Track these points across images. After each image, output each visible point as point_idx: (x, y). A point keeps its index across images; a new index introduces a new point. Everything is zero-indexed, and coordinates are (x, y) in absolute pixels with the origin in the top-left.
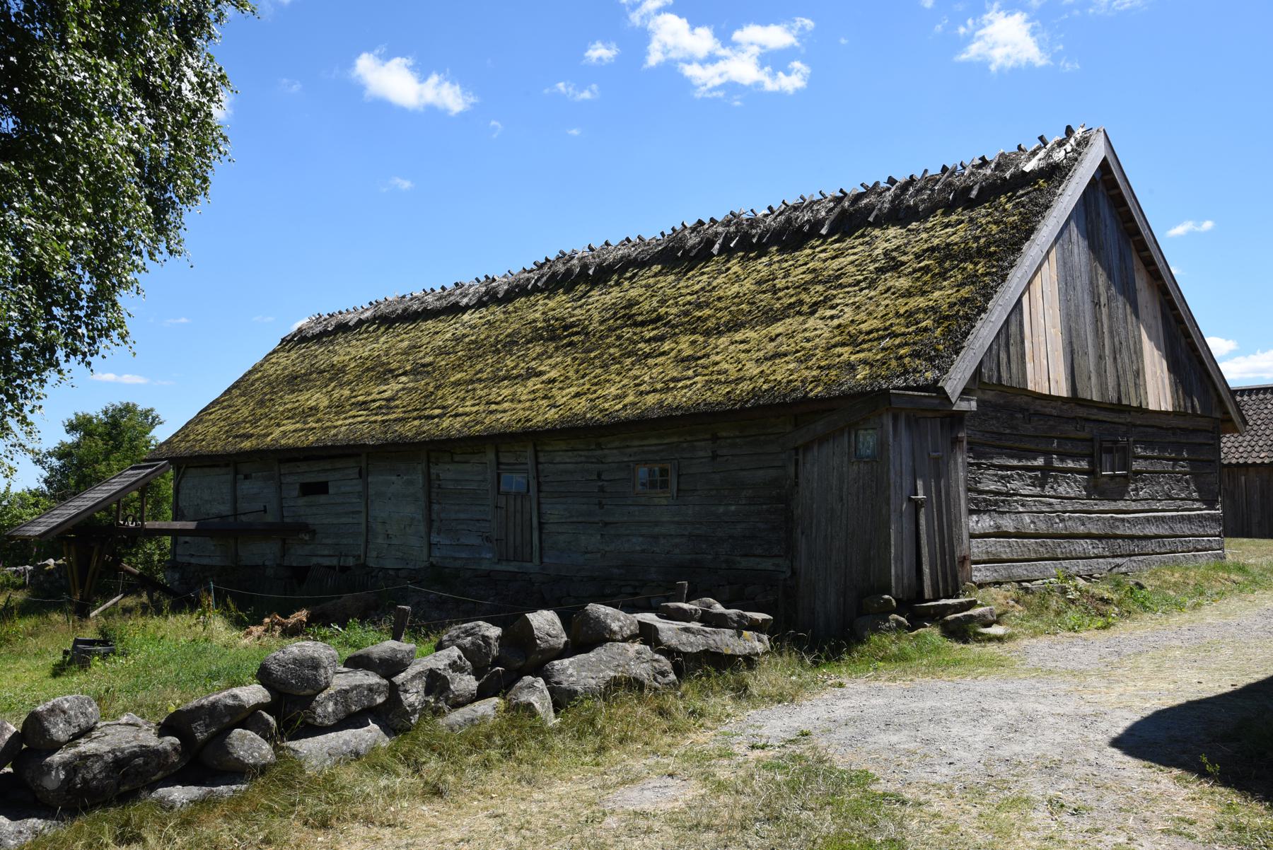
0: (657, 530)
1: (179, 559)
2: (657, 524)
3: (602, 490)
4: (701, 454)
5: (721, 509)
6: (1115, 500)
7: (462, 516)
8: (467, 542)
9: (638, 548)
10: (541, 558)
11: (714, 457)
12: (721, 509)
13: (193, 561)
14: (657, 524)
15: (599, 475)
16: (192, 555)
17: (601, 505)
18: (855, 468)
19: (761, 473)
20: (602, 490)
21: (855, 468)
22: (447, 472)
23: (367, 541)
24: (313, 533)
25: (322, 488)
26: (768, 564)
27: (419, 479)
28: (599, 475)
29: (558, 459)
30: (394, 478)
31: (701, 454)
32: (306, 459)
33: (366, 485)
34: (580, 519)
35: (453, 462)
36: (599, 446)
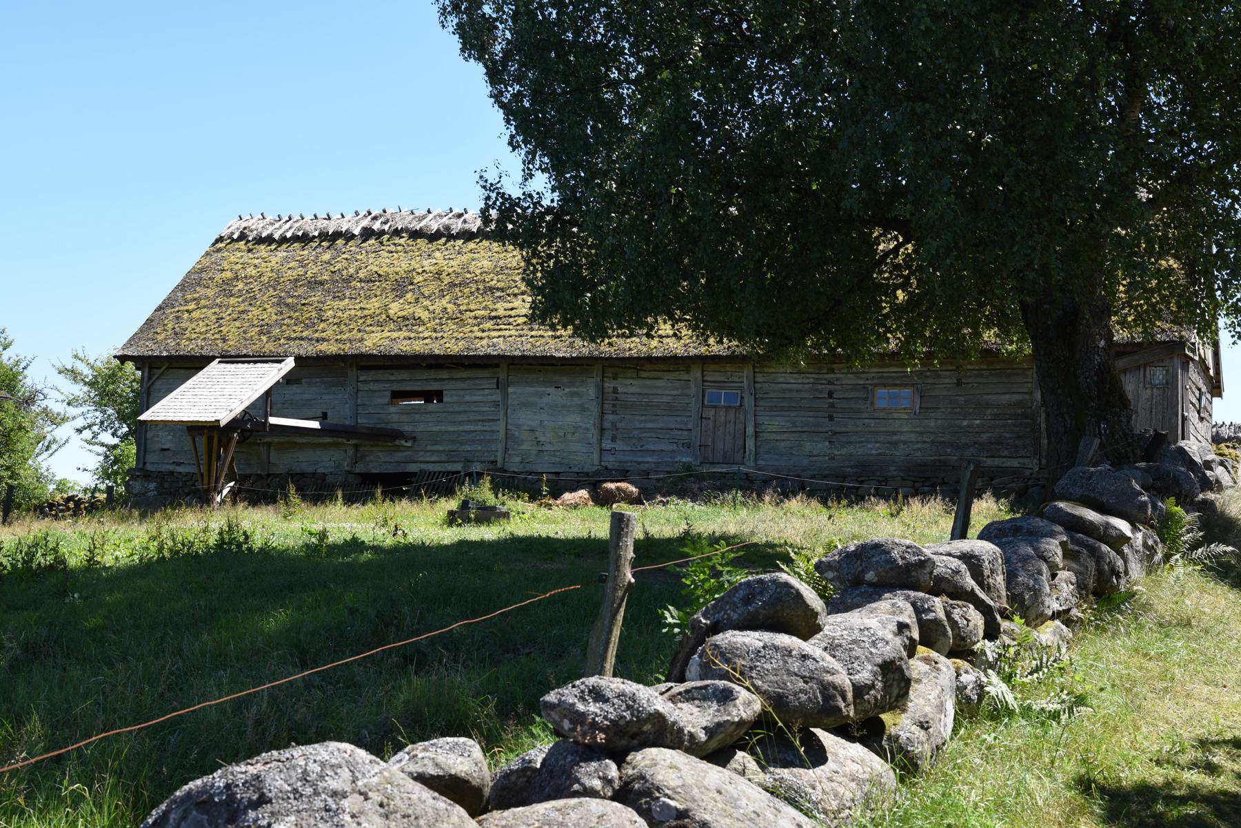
0: (895, 438)
1: (149, 467)
2: (895, 433)
3: (832, 406)
4: (947, 381)
5: (965, 423)
6: (617, 656)
7: (649, 425)
8: (652, 448)
9: (874, 452)
10: (756, 459)
11: (959, 383)
12: (965, 423)
13: (179, 469)
14: (895, 433)
15: (830, 394)
16: (179, 464)
17: (831, 418)
18: (1149, 392)
19: (1007, 397)
20: (832, 406)
21: (1149, 392)
22: (629, 387)
23: (506, 449)
24: (414, 439)
25: (439, 395)
26: (1014, 463)
27: (592, 392)
28: (830, 394)
29: (781, 380)
30: (551, 390)
31: (947, 381)
32: (430, 367)
33: (505, 395)
34: (805, 429)
35: (638, 377)
36: (832, 371)
